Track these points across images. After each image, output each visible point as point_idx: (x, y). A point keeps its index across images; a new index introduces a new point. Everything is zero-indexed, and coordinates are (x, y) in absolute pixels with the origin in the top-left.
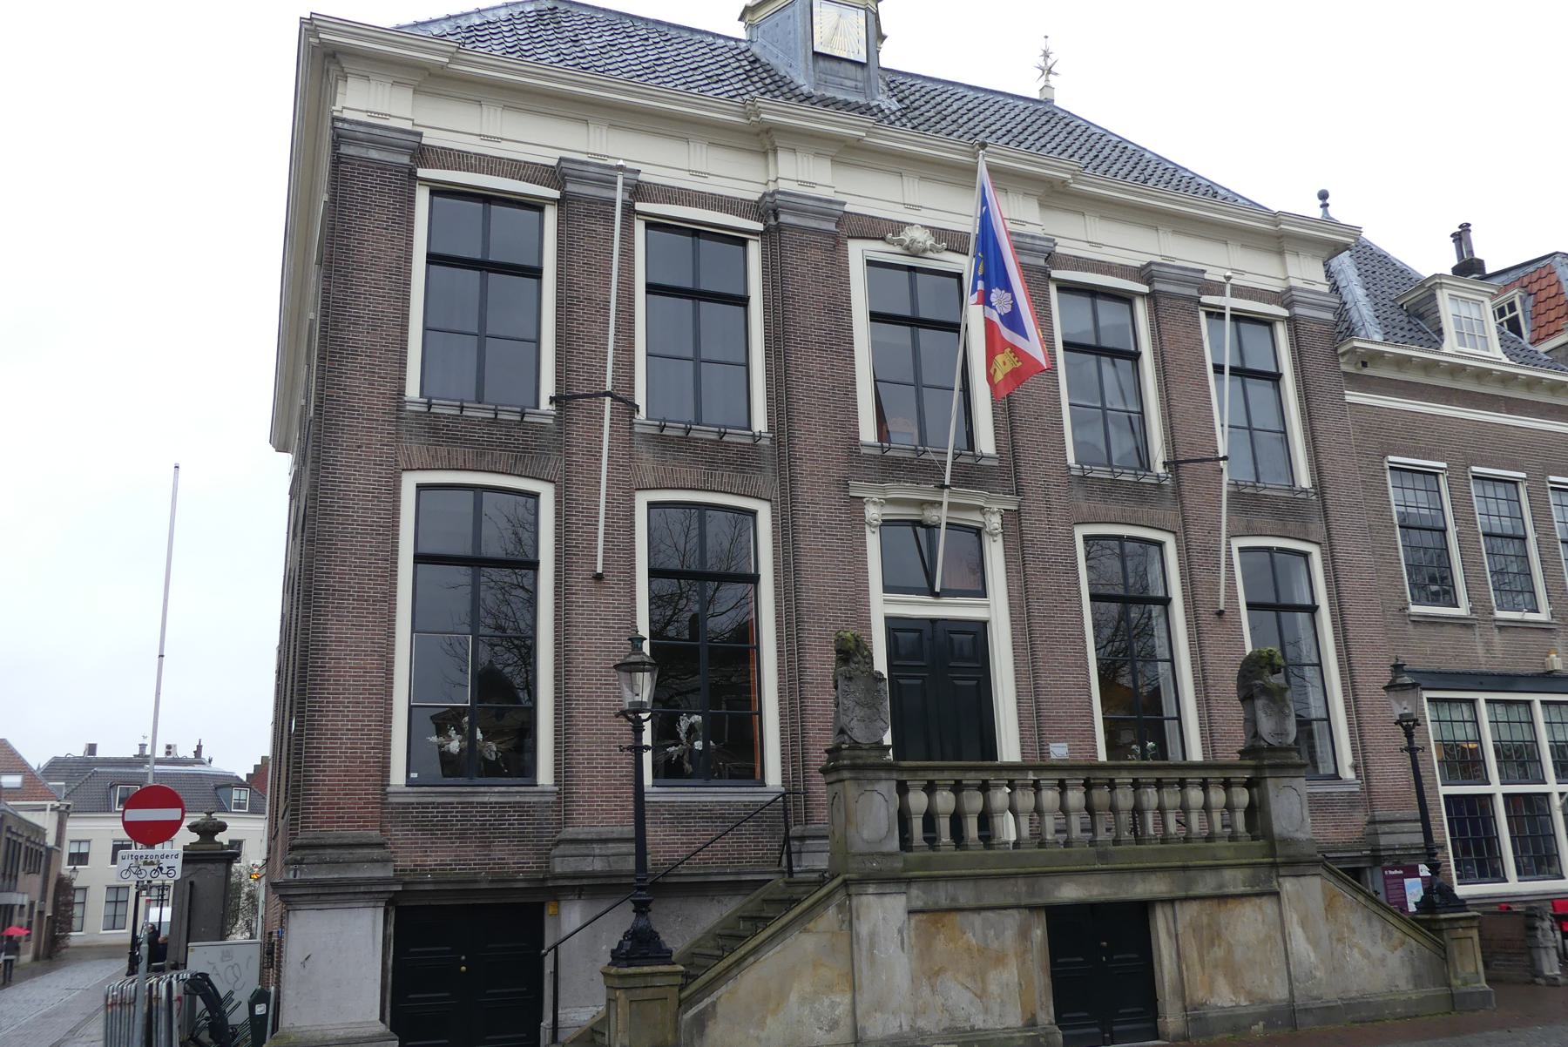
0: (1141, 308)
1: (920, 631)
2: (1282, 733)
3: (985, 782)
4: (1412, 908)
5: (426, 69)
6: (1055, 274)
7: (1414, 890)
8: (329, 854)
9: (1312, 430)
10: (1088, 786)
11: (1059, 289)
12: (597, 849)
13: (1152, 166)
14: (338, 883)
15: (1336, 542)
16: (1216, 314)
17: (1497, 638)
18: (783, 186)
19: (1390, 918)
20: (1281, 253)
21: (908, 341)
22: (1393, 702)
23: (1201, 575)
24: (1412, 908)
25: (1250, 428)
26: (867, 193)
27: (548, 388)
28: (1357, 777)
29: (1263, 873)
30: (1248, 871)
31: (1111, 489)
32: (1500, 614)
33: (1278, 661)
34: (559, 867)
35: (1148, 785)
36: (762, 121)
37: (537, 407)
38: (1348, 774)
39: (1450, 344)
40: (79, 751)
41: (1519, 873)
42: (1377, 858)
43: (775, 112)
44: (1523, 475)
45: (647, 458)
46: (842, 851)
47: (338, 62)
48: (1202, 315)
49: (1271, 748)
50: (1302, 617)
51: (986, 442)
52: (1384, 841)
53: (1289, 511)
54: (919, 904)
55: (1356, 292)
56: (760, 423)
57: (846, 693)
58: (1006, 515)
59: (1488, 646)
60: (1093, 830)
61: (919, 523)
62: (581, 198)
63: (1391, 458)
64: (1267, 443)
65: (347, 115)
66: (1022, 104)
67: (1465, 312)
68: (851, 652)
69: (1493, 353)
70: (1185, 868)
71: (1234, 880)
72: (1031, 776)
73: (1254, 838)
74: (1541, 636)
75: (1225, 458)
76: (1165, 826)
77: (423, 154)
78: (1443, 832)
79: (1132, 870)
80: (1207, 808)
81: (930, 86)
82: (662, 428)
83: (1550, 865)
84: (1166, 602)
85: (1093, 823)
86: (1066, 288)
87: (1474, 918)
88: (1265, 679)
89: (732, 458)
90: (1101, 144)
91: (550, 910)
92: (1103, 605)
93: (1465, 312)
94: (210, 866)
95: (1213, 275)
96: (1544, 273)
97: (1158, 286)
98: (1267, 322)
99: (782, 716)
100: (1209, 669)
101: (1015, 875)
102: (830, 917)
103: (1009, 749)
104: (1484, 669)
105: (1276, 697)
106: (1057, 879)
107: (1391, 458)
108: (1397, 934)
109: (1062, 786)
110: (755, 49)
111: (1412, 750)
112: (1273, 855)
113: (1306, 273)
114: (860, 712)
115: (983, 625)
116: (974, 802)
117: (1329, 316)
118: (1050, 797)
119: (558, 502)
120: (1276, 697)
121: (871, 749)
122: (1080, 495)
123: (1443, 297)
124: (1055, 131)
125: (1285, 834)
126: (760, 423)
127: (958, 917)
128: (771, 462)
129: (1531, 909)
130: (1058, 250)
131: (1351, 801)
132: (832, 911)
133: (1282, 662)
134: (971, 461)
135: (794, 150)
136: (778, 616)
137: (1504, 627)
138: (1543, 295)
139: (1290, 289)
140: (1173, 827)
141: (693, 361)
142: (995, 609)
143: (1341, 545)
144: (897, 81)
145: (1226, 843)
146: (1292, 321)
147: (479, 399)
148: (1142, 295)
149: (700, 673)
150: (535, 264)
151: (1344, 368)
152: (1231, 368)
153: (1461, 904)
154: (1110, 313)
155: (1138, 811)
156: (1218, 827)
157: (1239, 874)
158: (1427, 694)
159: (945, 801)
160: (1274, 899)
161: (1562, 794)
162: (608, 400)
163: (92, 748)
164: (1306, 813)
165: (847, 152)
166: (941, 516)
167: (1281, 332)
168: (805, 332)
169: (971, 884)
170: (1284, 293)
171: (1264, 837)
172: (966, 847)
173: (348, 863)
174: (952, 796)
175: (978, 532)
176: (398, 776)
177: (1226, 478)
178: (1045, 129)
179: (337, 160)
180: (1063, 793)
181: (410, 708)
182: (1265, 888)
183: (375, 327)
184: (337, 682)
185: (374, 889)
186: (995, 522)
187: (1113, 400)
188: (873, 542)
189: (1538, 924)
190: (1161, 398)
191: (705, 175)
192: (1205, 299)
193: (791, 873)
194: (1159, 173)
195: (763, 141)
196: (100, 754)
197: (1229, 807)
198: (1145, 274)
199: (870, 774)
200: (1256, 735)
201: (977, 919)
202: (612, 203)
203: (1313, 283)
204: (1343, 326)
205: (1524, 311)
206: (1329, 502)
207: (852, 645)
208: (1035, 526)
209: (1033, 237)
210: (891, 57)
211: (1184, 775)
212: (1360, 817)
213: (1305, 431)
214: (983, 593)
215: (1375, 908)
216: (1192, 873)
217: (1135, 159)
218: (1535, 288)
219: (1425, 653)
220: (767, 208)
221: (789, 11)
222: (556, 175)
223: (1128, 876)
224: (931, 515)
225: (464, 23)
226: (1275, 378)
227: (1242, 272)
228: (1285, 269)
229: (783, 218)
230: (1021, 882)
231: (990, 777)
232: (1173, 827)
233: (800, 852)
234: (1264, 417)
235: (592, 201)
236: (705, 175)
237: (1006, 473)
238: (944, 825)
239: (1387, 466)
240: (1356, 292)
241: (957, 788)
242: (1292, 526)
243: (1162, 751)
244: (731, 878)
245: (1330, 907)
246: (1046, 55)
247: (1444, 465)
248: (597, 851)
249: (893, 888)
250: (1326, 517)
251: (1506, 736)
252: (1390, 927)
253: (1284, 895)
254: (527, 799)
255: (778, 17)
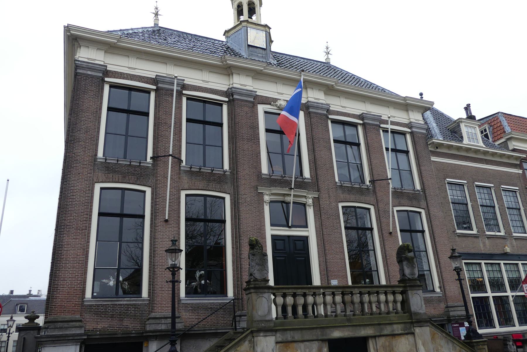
0: (360, 129)
1: (284, 240)
2: (413, 274)
3: (305, 293)
4: (463, 338)
5: (110, 44)
6: (330, 117)
7: (463, 332)
8: (59, 325)
9: (420, 170)
10: (343, 294)
11: (332, 122)
12: (163, 321)
13: (363, 83)
14: (61, 336)
15: (430, 208)
16: (386, 131)
17: (487, 241)
18: (235, 86)
19: (455, 342)
20: (407, 111)
21: (279, 140)
22: (453, 263)
23: (383, 220)
24: (463, 338)
25: (399, 169)
26: (264, 89)
27: (150, 154)
28: (441, 291)
29: (408, 326)
30: (402, 325)
31: (351, 190)
32: (487, 233)
33: (411, 247)
34: (148, 328)
35: (365, 294)
36: (227, 64)
37: (146, 161)
38: (438, 290)
39: (466, 141)
40: (7, 293)
41: (500, 325)
42: (449, 320)
43: (231, 61)
44: (493, 185)
45: (185, 178)
46: (251, 321)
47: (78, 42)
48: (381, 131)
49: (409, 279)
50: (419, 235)
51: (307, 174)
52: (452, 314)
53: (413, 198)
54: (280, 340)
55: (433, 125)
56: (226, 167)
57: (252, 260)
58: (314, 199)
59: (484, 243)
60: (345, 311)
61: (283, 202)
62: (162, 87)
63: (448, 180)
64: (405, 174)
65: (80, 59)
66: (319, 64)
67: (470, 131)
68: (256, 246)
69: (480, 144)
70: (379, 324)
71: (398, 329)
72: (322, 291)
73: (404, 313)
74: (502, 241)
75: (390, 179)
76: (372, 308)
77: (107, 73)
78: (472, 311)
79: (360, 326)
80: (387, 302)
81: (288, 57)
82: (191, 168)
83: (510, 321)
84: (371, 229)
85: (345, 309)
86: (334, 122)
87: (485, 341)
88: (406, 255)
89: (216, 179)
90: (346, 76)
91: (145, 345)
92: (350, 231)
93: (470, 131)
94: (32, 332)
95: (384, 118)
96: (495, 119)
97: (366, 121)
98: (403, 134)
99: (234, 271)
100: (387, 253)
101: (316, 328)
102: (246, 345)
103: (317, 281)
104: (483, 252)
105: (410, 261)
106: (332, 329)
107: (448, 180)
108: (458, 348)
109: (334, 294)
110: (229, 44)
111: (460, 280)
112: (412, 319)
113: (416, 117)
114: (257, 267)
115: (307, 237)
116: (301, 301)
117: (425, 132)
118: (329, 298)
119: (152, 194)
120: (410, 261)
121: (262, 281)
122: (340, 192)
123: (462, 126)
124: (330, 72)
125: (416, 311)
126: (226, 167)
127: (295, 345)
128: (230, 181)
129: (504, 337)
130: (331, 109)
131: (439, 300)
132: (247, 343)
133: (412, 248)
134: (301, 180)
135: (239, 74)
136: (232, 235)
137: (490, 237)
138: (496, 126)
139: (411, 122)
140: (374, 309)
141: (205, 146)
142: (311, 233)
143: (432, 209)
144: (277, 55)
145: (394, 315)
146: (412, 133)
147: (125, 157)
148: (360, 124)
149: (205, 258)
150: (147, 111)
151: (430, 149)
152: (391, 149)
153: (480, 336)
154: (349, 131)
155: (362, 303)
156: (391, 309)
157: (399, 326)
158: (464, 261)
159: (290, 300)
160: (413, 335)
161: (513, 296)
162: (170, 157)
163: (12, 292)
164: (423, 303)
165: (257, 75)
166: (291, 199)
167: (408, 137)
168: (243, 135)
169: (300, 332)
170: (409, 124)
171: (408, 312)
172: (297, 318)
173: (67, 328)
174: (292, 298)
175: (304, 205)
176: (88, 294)
177: (391, 186)
178: (327, 71)
179: (76, 74)
180: (334, 298)
181: (95, 269)
182: (409, 331)
183: (87, 132)
184: (66, 260)
185: (76, 338)
186: (310, 201)
187: (351, 160)
188: (267, 209)
189: (508, 343)
190: (368, 159)
191: (207, 82)
192: (382, 126)
193: (236, 329)
194: (365, 85)
195: (228, 71)
196: (15, 293)
197: (395, 302)
198: (361, 117)
199: (261, 291)
200: (404, 275)
201: (302, 345)
202: (173, 90)
203: (419, 120)
204: (429, 135)
205: (489, 132)
206: (427, 195)
207: (255, 242)
208: (324, 203)
209: (322, 104)
210: (274, 48)
211: (378, 289)
212: (443, 305)
213: (418, 170)
214: (306, 227)
215: (449, 338)
216: (382, 326)
217: (357, 81)
218: (493, 124)
219: (462, 247)
220: (229, 93)
221: (240, 32)
222: (155, 81)
223: (358, 328)
224: (287, 199)
225: (126, 32)
226: (407, 152)
227: (394, 117)
228: (409, 116)
229: (235, 97)
230: (318, 330)
231: (307, 291)
232: (374, 309)
233: (240, 321)
234: (404, 166)
235: (167, 90)
236: (207, 82)
237: (314, 184)
238: (290, 309)
239: (446, 182)
240: (433, 125)
241: (294, 296)
242: (414, 203)
243: (372, 282)
244: (213, 331)
245: (433, 338)
246: (327, 48)
247: (466, 182)
248: (163, 322)
249: (270, 334)
250: (426, 199)
251: (492, 276)
252: (455, 345)
253: (416, 334)
254: (137, 303)
255: (236, 34)
